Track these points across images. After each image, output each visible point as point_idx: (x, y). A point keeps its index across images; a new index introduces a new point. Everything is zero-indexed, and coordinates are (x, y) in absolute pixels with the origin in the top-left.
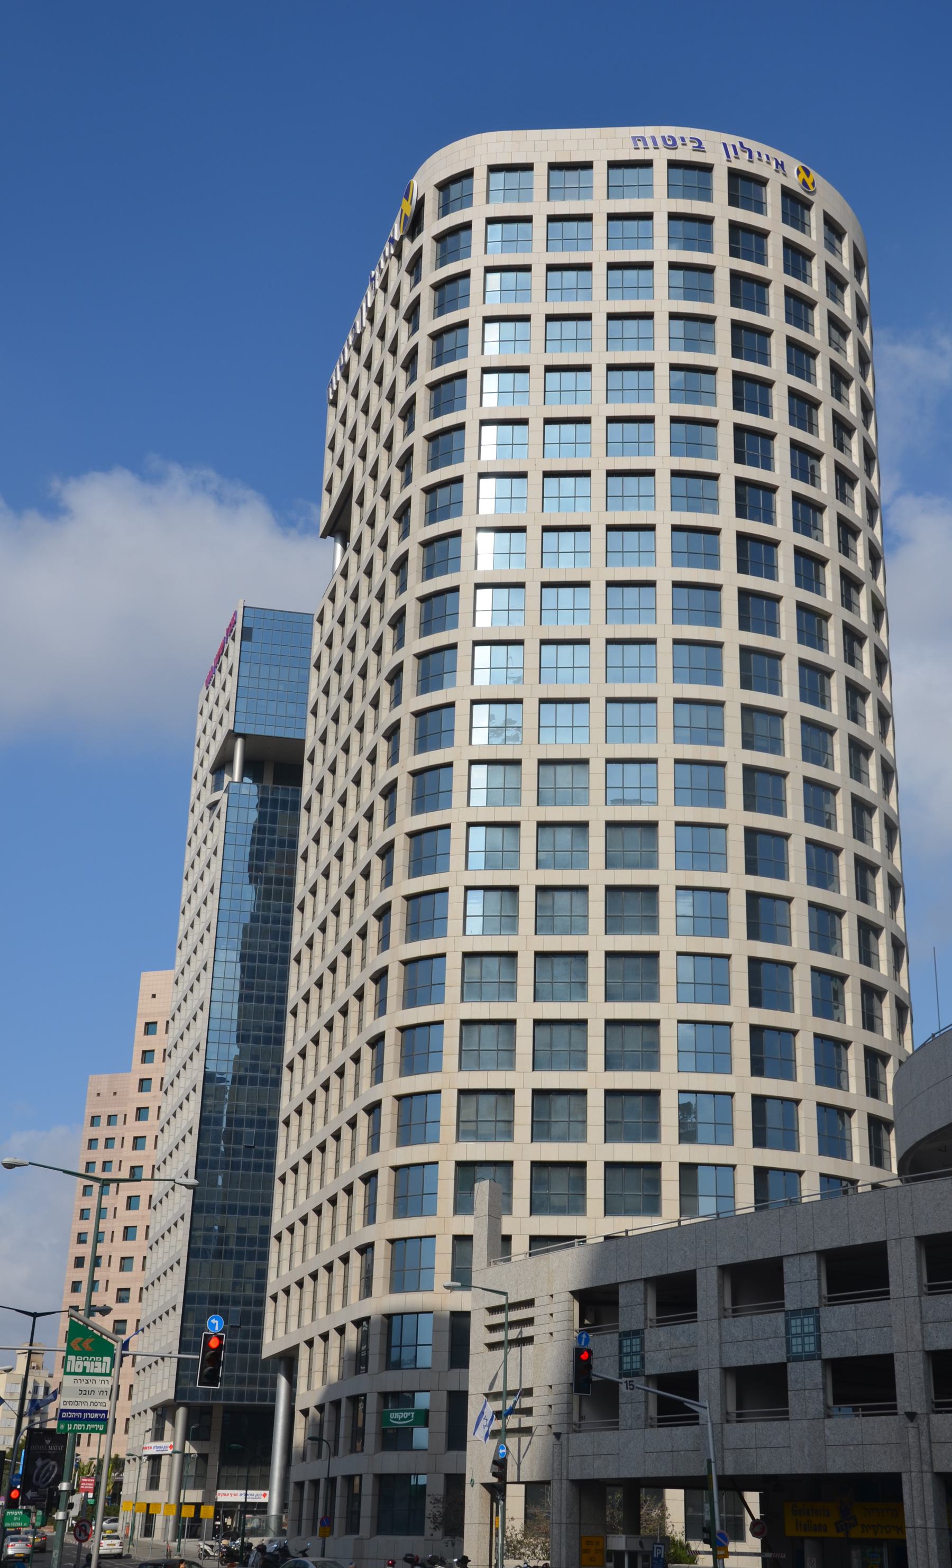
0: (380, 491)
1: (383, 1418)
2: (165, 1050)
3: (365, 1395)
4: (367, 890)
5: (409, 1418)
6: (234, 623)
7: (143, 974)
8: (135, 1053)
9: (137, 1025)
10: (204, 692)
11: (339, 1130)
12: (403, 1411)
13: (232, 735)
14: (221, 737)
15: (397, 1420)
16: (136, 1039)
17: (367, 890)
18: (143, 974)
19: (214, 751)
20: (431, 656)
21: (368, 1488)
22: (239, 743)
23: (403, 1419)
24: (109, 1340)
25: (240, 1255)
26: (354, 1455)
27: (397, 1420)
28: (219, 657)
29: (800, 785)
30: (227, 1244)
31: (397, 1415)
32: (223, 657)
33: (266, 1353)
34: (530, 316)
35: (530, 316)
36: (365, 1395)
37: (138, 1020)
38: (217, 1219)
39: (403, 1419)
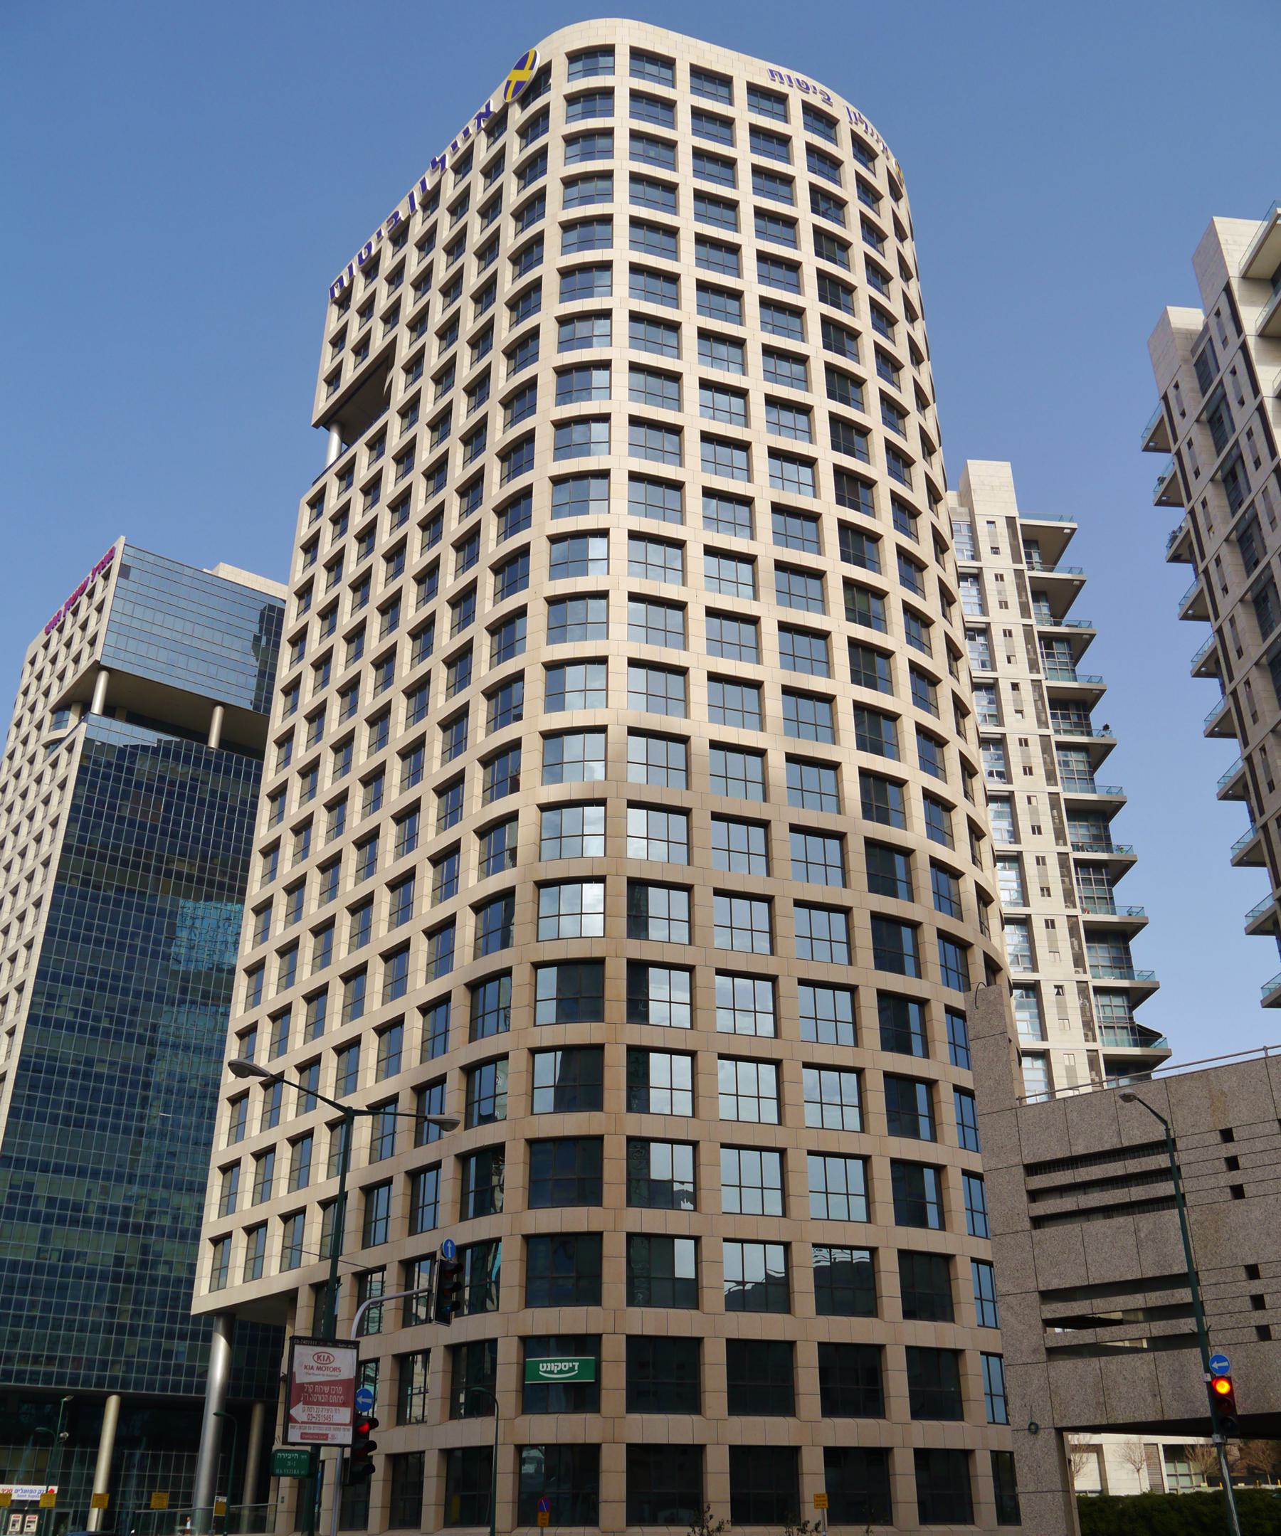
1: (524, 1370)
3: (494, 1341)
5: (571, 1370)
7: (1008, 464)
12: (561, 1361)
13: (97, 667)
14: (85, 664)
15: (552, 1372)
18: (1008, 464)
20: (569, 604)
21: (432, 1467)
22: (102, 679)
23: (561, 1372)
24: (472, 1186)
26: (401, 1428)
27: (552, 1372)
29: (862, 848)
31: (551, 1367)
33: (196, 1309)
34: (609, 415)
35: (609, 415)
36: (494, 1341)
39: (561, 1372)
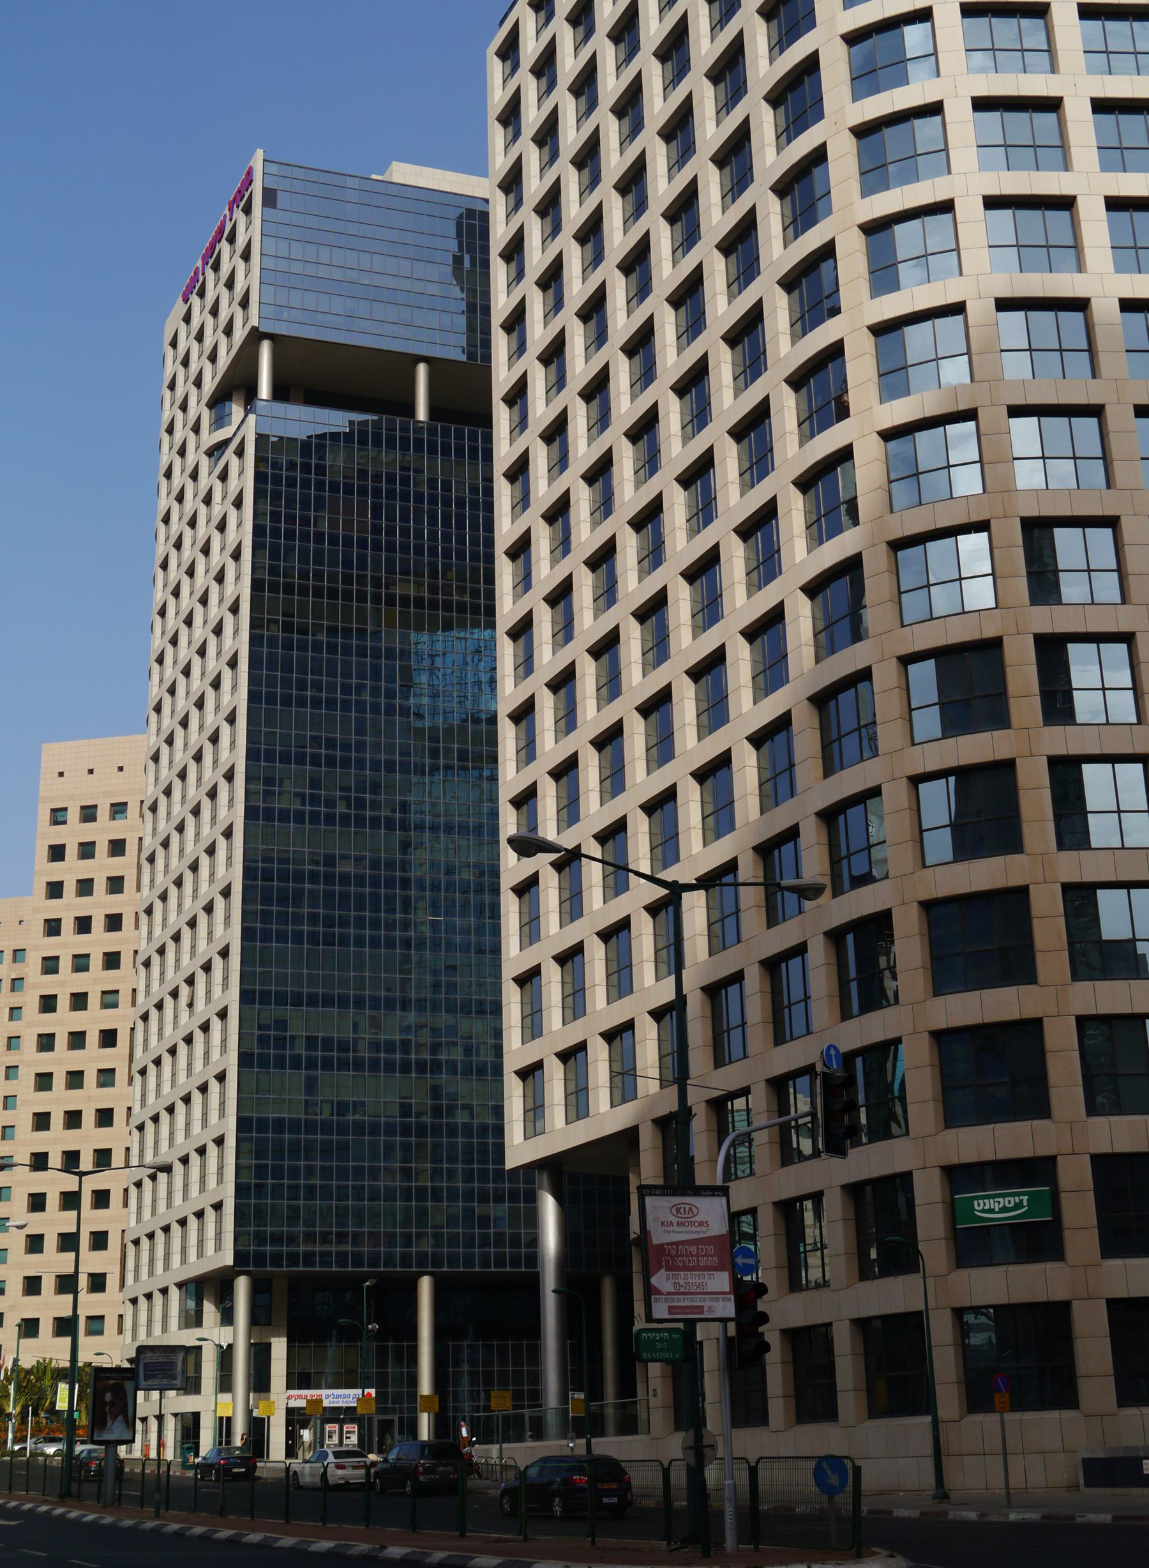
0: (180, 359)
1: (953, 1211)
2: (142, 802)
4: (169, 806)
5: (1019, 1206)
6: (249, 181)
8: (38, 849)
9: (40, 812)
10: (180, 308)
11: (191, 1034)
12: (1003, 1196)
13: (256, 336)
16: (39, 830)
17: (169, 806)
18: (44, 746)
19: (224, 359)
21: (844, 1342)
23: (1004, 1209)
25: (311, 1064)
28: (218, 239)
30: (292, 1048)
31: (990, 1204)
32: (224, 246)
37: (41, 806)
38: (273, 1011)
